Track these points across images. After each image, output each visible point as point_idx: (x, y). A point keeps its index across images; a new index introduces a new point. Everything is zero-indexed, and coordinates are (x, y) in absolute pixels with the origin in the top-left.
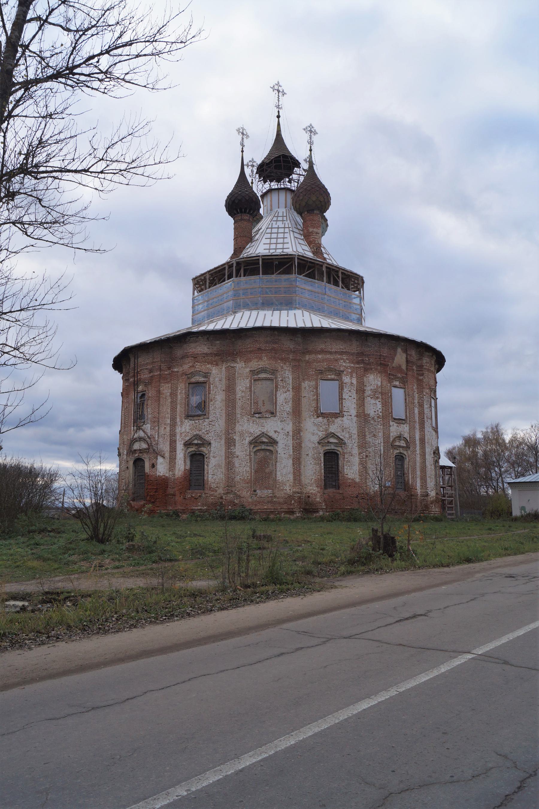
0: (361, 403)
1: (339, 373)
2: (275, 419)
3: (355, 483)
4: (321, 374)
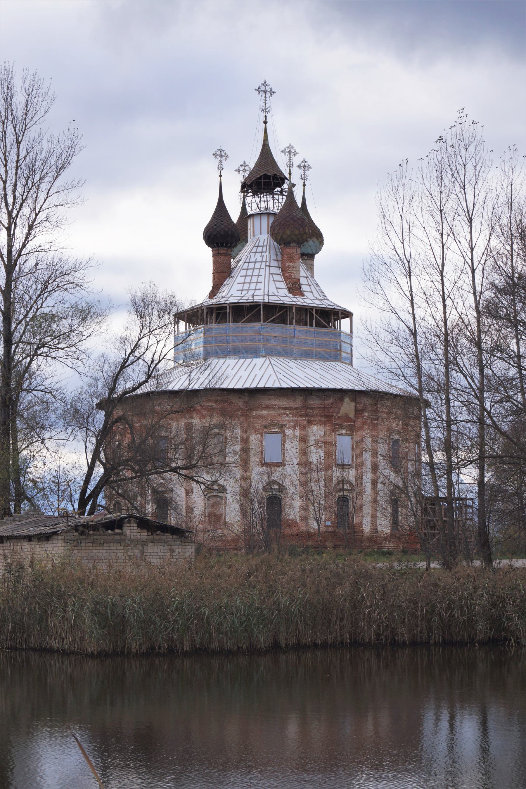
0: (304, 452)
1: (282, 427)
2: (174, 489)
3: (297, 523)
4: (266, 428)
